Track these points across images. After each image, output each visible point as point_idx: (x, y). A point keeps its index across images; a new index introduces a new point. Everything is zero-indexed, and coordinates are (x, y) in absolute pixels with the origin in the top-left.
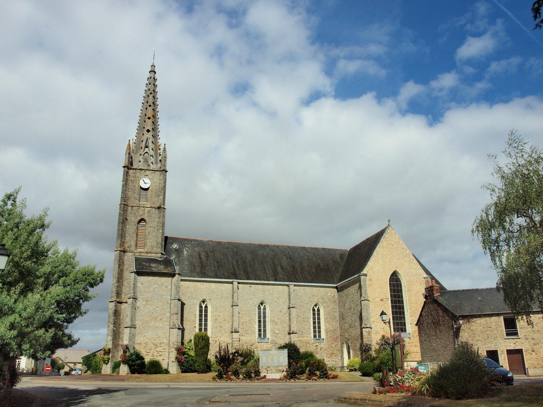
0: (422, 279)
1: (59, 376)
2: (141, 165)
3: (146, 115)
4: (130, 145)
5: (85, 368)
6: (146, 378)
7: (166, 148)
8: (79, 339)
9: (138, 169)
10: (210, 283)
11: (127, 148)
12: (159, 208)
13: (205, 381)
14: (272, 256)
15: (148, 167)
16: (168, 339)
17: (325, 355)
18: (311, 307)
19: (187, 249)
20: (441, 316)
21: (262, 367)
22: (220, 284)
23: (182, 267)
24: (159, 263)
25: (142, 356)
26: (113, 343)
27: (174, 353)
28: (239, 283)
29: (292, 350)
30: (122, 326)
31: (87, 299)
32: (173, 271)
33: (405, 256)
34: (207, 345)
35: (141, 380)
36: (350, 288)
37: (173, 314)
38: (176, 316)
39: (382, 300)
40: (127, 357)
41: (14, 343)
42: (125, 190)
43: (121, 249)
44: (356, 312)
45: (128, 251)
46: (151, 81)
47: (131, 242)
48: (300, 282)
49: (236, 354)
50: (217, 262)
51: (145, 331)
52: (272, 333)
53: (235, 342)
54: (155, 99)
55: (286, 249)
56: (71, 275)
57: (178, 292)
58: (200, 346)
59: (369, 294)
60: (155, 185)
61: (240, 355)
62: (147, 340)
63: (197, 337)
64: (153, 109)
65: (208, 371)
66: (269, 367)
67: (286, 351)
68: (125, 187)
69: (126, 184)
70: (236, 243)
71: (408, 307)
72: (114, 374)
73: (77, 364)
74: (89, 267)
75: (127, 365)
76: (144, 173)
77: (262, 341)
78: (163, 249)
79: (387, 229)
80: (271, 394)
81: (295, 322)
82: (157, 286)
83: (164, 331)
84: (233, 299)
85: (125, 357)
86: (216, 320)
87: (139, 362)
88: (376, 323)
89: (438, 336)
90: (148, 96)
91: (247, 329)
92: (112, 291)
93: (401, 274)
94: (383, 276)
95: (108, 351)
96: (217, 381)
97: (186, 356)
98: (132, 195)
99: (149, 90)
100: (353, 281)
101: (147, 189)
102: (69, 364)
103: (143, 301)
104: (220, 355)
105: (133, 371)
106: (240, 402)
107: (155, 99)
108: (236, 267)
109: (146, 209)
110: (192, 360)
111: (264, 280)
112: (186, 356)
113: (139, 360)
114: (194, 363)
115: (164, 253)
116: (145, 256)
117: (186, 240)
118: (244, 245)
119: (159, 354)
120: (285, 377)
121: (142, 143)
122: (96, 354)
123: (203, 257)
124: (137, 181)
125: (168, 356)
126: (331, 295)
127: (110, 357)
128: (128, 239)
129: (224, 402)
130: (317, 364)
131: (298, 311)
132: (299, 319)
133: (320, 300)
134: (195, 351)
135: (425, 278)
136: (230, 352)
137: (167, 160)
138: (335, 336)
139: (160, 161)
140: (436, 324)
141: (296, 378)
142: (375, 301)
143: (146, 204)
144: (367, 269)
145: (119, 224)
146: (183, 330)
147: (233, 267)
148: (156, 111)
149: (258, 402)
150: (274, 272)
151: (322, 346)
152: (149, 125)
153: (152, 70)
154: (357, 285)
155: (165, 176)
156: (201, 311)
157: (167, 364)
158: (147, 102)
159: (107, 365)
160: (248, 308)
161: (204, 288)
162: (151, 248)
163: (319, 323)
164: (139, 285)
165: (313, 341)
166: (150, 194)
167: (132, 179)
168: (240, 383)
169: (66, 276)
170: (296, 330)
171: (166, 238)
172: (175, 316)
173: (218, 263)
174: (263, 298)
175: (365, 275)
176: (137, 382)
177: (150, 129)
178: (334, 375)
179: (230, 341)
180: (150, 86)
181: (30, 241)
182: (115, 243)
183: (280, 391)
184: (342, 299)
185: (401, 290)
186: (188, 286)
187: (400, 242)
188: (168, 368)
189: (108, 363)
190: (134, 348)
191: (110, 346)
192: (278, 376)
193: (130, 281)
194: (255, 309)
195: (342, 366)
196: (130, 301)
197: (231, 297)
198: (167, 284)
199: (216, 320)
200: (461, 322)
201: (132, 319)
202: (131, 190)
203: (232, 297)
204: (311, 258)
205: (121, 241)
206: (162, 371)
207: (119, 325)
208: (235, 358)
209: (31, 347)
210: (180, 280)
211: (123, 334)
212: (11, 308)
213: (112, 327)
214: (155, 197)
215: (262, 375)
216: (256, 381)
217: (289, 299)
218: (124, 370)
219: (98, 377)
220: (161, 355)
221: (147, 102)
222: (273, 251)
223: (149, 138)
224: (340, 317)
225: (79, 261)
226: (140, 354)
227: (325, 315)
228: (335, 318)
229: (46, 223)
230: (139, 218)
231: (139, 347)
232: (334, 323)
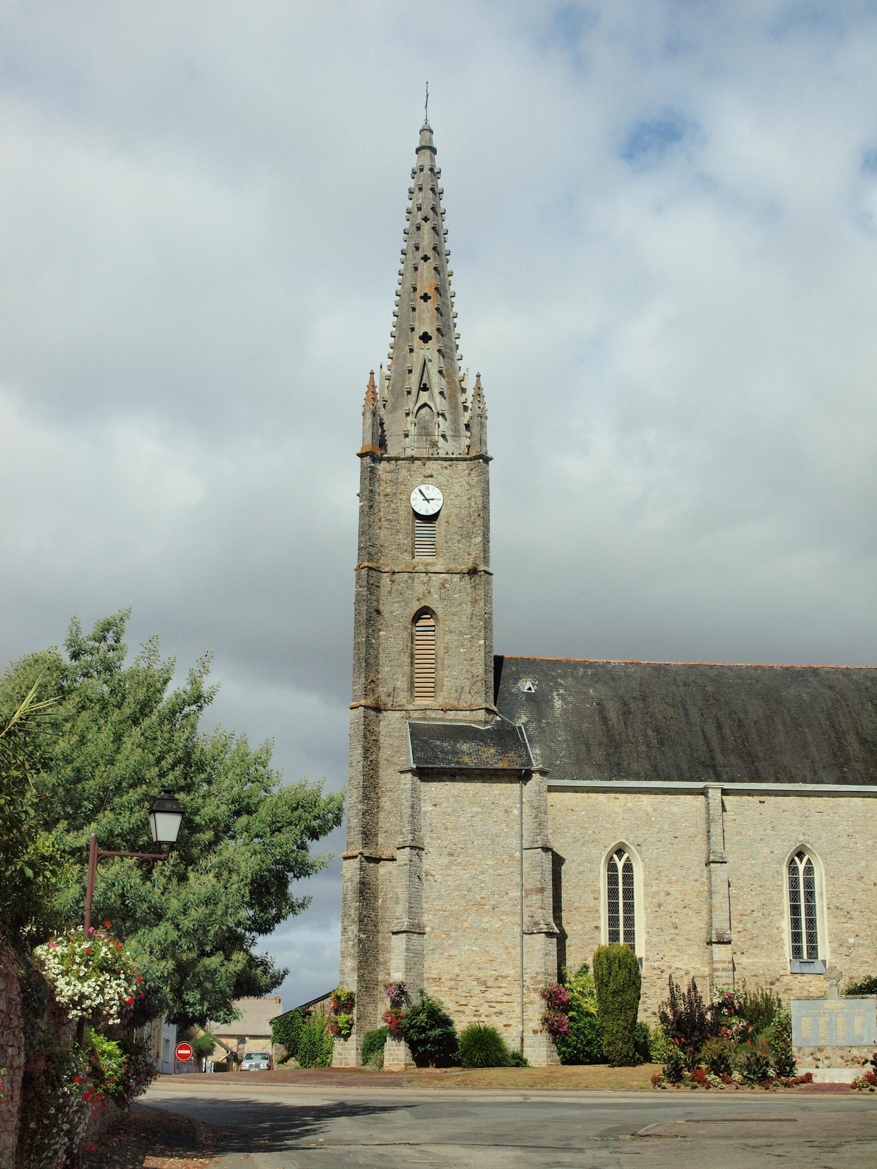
1: (198, 1074)
2: (412, 447)
3: (415, 289)
4: (374, 387)
5: (279, 1051)
7: (483, 386)
8: (286, 972)
9: (403, 459)
10: (637, 796)
13: (630, 1089)
14: (829, 703)
15: (431, 451)
16: (519, 964)
19: (562, 691)
23: (549, 747)
24: (482, 741)
25: (444, 1015)
26: (361, 978)
27: (537, 1006)
28: (725, 792)
30: (383, 927)
32: (523, 765)
34: (634, 983)
35: (448, 1083)
37: (529, 892)
38: (539, 896)
40: (402, 1018)
41: (168, 989)
43: (369, 702)
45: (389, 706)
47: (397, 679)
49: (725, 1010)
50: (657, 730)
51: (451, 942)
52: (835, 944)
54: (438, 234)
56: (263, 811)
58: (612, 986)
60: (457, 502)
61: (735, 1011)
62: (457, 970)
64: (436, 269)
65: (639, 1059)
66: (820, 1050)
68: (368, 515)
69: (371, 507)
70: (712, 667)
72: (368, 1068)
73: (247, 1039)
74: (304, 786)
75: (403, 1042)
76: (422, 470)
77: (806, 969)
78: (492, 697)
80: (800, 1121)
82: (479, 810)
83: (507, 943)
84: (709, 843)
85: (397, 1018)
87: (438, 1031)
90: (418, 228)
91: (756, 932)
92: (349, 828)
95: (348, 1000)
96: (664, 1088)
97: (571, 1014)
98: (390, 538)
99: (419, 209)
101: (433, 518)
102: (224, 1041)
105: (421, 1060)
106: (714, 1137)
107: (438, 234)
109: (434, 577)
110: (592, 1026)
111: (805, 781)
112: (571, 1014)
113: (438, 1027)
114: (598, 1036)
115: (495, 709)
116: (440, 719)
117: (556, 663)
118: (739, 673)
119: (495, 1010)
122: (311, 1009)
123: (613, 714)
125: (520, 1015)
127: (355, 1019)
128: (388, 672)
129: (672, 1137)
134: (600, 999)
136: (707, 1003)
137: (489, 423)
139: (467, 426)
143: (434, 564)
146: (561, 938)
147: (708, 743)
149: (760, 1137)
150: (835, 755)
152: (428, 320)
153: (424, 144)
155: (485, 473)
156: (612, 880)
157: (519, 1039)
158: (417, 248)
159: (346, 1040)
160: (758, 870)
164: (426, 807)
167: (388, 490)
168: (731, 1093)
169: (249, 813)
171: (499, 661)
174: (802, 838)
176: (435, 1088)
177: (432, 332)
179: (706, 970)
180: (421, 194)
181: (176, 744)
183: (833, 1114)
186: (570, 808)
188: (522, 1051)
189: (349, 1035)
190: (422, 992)
192: (848, 1075)
193: (399, 797)
196: (403, 856)
198: (509, 802)
199: (659, 906)
202: (385, 524)
203: (705, 838)
205: (366, 678)
206: (504, 1059)
207: (375, 926)
208: (723, 1021)
209: (203, 999)
210: (546, 788)
211: (389, 952)
212: (155, 908)
213: (356, 933)
215: (800, 1071)
216: (781, 1089)
219: (326, 1077)
220: (501, 1013)
221: (417, 248)
222: (830, 687)
223: (430, 361)
225: (280, 771)
226: (440, 1010)
229: (205, 689)
230: (416, 607)
231: (435, 988)
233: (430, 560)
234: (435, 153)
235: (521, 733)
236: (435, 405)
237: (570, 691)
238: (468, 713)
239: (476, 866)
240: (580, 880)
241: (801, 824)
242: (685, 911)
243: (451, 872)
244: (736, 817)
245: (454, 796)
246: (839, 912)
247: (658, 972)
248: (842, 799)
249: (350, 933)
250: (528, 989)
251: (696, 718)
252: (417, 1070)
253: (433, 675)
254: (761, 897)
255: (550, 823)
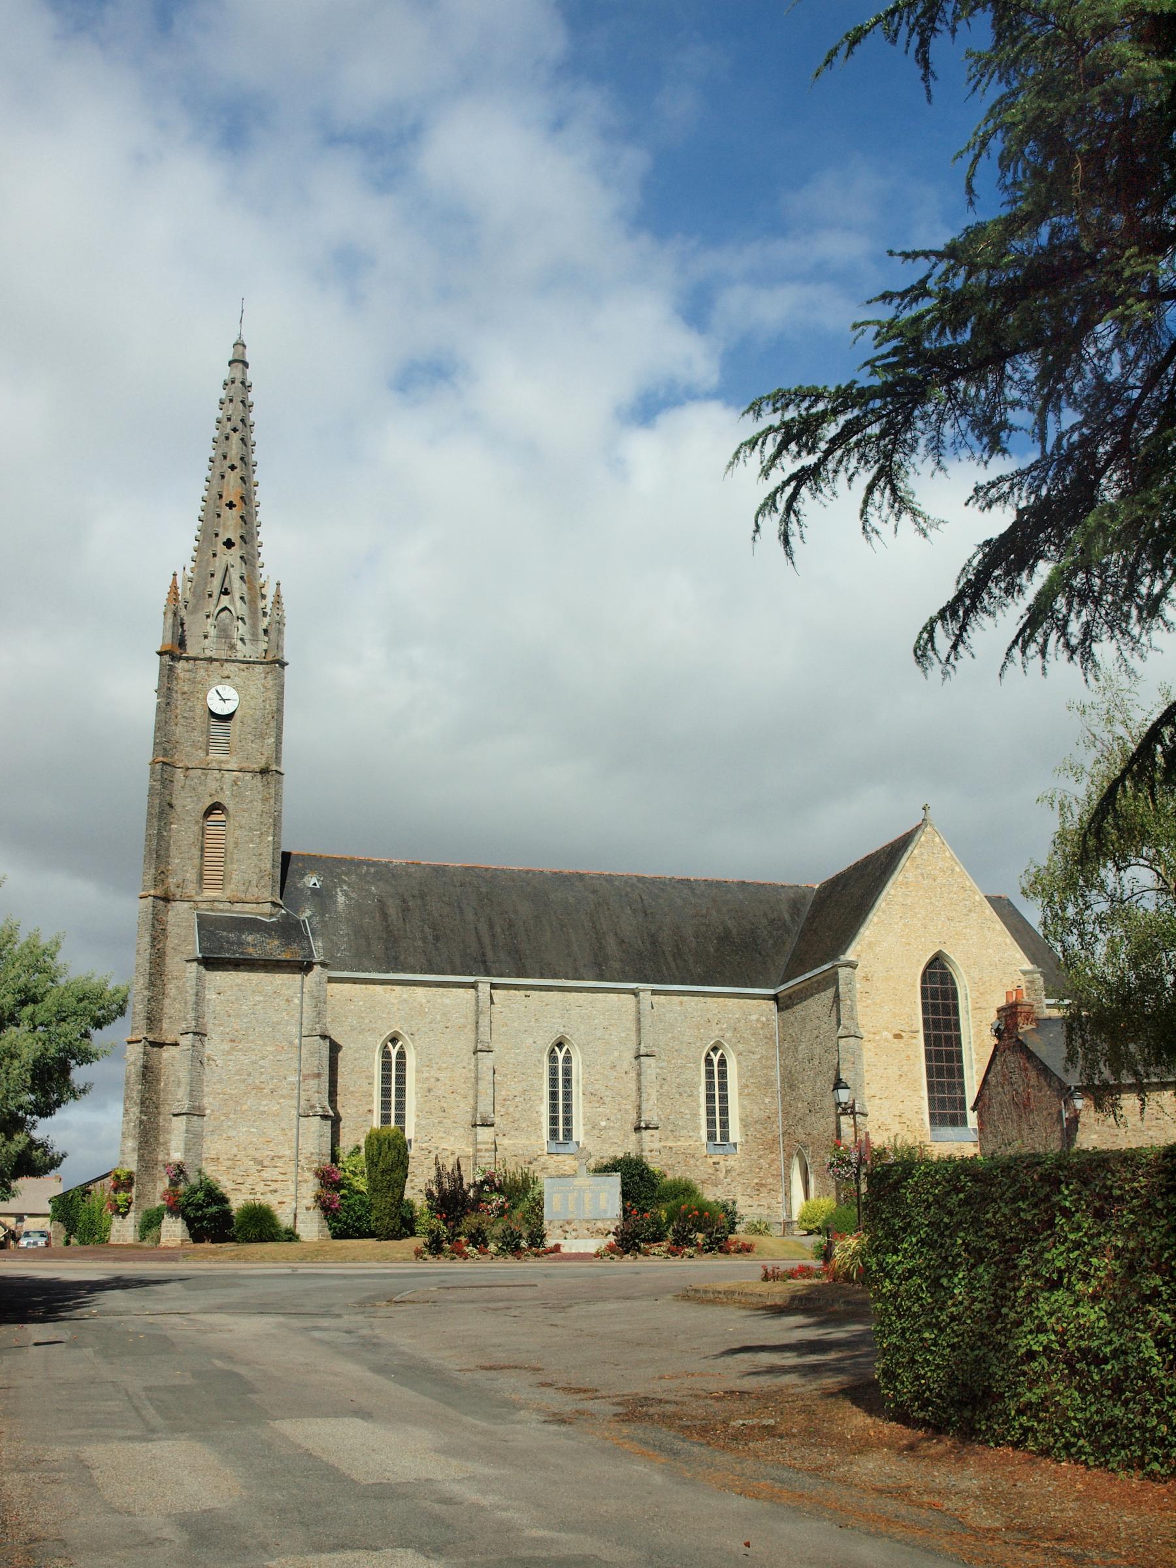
0: (1016, 977)
3: (221, 496)
4: (176, 588)
6: (235, 1253)
7: (282, 594)
9: (201, 660)
10: (412, 988)
11: (167, 596)
12: (264, 772)
13: (395, 1260)
14: (593, 907)
15: (229, 653)
16: (294, 1145)
17: (739, 1189)
18: (701, 1053)
19: (345, 888)
20: (1033, 1086)
21: (550, 1222)
22: (441, 990)
23: (332, 941)
24: (267, 933)
26: (141, 1158)
27: (310, 1185)
28: (493, 986)
29: (633, 1176)
31: (86, 1057)
32: (305, 957)
33: (970, 911)
34: (402, 1163)
35: (222, 1257)
36: (810, 1001)
37: (306, 1077)
38: (316, 1081)
39: (898, 1036)
40: (180, 1196)
42: (166, 722)
43: (158, 893)
44: (826, 1070)
45: (178, 897)
46: (233, 390)
47: (187, 871)
48: (671, 983)
49: (486, 1188)
50: (434, 928)
51: (230, 1123)
53: (482, 1154)
55: (632, 886)
56: (49, 1001)
57: (320, 1014)
58: (381, 1166)
59: (861, 1019)
62: (234, 1151)
63: (375, 1140)
64: (242, 478)
65: (405, 1233)
66: (569, 1223)
67: (616, 1179)
68: (164, 712)
70: (487, 869)
71: (974, 1056)
72: (145, 1244)
73: (25, 1217)
75: (180, 1219)
76: (219, 671)
77: (561, 1149)
78: (279, 891)
79: (920, 832)
81: (654, 1097)
82: (262, 998)
83: (283, 1125)
84: (477, 1034)
85: (175, 1196)
86: (429, 1091)
87: (214, 1209)
88: (880, 1101)
89: (1026, 1142)
90: (227, 438)
91: (517, 1115)
93: (957, 963)
94: (902, 968)
95: (128, 1179)
96: (425, 1259)
99: (229, 419)
100: (818, 982)
101: (228, 718)
103: (222, 1040)
104: (441, 1190)
105: (197, 1236)
106: (461, 1302)
108: (487, 940)
110: (362, 1203)
111: (567, 978)
112: (343, 1192)
113: (215, 1204)
114: (367, 1212)
115: (281, 903)
116: (226, 911)
117: (341, 861)
118: (512, 875)
119: (271, 1188)
120: (611, 1249)
121: (211, 582)
122: (91, 1187)
123: (392, 911)
124: (199, 695)
126: (758, 1020)
130: (696, 1213)
131: (664, 1064)
132: (666, 1087)
133: (729, 1035)
135: (1025, 973)
137: (286, 630)
138: (770, 1137)
139: (266, 631)
140: (1021, 1106)
141: (639, 1250)
142: (877, 1038)
143: (227, 762)
144: (859, 948)
145: (149, 821)
146: (336, 1121)
147: (479, 939)
148: (249, 481)
149: (502, 1300)
151: (732, 1162)
153: (236, 357)
154: (830, 993)
156: (386, 1067)
158: (225, 457)
159: (124, 1218)
160: (521, 1058)
161: (396, 1001)
162: (243, 888)
163: (724, 1098)
164: (211, 995)
165: (705, 1151)
166: (238, 733)
167: (186, 689)
170: (656, 1118)
171: (286, 857)
172: (312, 1082)
173: (435, 930)
174: (562, 1030)
175: (852, 965)
176: (210, 1262)
177: (235, 539)
178: (744, 1245)
180: (231, 405)
182: (140, 874)
184: (790, 1031)
185: (956, 1007)
187: (957, 869)
188: (295, 1227)
190: (200, 1172)
191: (132, 1165)
192: (592, 1245)
194: (539, 1061)
195: (789, 1220)
196: (186, 1041)
197: (471, 1027)
199: (429, 1091)
200: (1079, 1104)
201: (191, 1090)
203: (474, 1028)
204: (704, 911)
205: (157, 869)
206: (277, 1234)
207: (157, 1108)
213: (138, 1114)
214: (252, 742)
215: (550, 1243)
216: (532, 1259)
217: (639, 1030)
218: (175, 1231)
220: (276, 1191)
221: (225, 457)
222: (594, 892)
223: (233, 566)
224: (782, 1081)
225: (68, 963)
226: (217, 1189)
227: (740, 1077)
228: (769, 1083)
230: (208, 802)
231: (213, 1168)
232: (767, 1100)
233: (223, 757)
234: (247, 367)
235: (305, 926)
236: (235, 609)
237: (354, 888)
238: (255, 905)
239: (256, 1052)
240: (355, 1066)
241: (562, 1017)
242: (453, 1096)
243: (232, 1057)
244: (503, 1009)
245: (237, 985)
246: (593, 1098)
247: (426, 1152)
248: (600, 995)
249: (132, 1115)
250: (303, 1168)
251: (470, 916)
252: (193, 1246)
253: (222, 868)
254: (523, 1083)
255: (329, 1012)
